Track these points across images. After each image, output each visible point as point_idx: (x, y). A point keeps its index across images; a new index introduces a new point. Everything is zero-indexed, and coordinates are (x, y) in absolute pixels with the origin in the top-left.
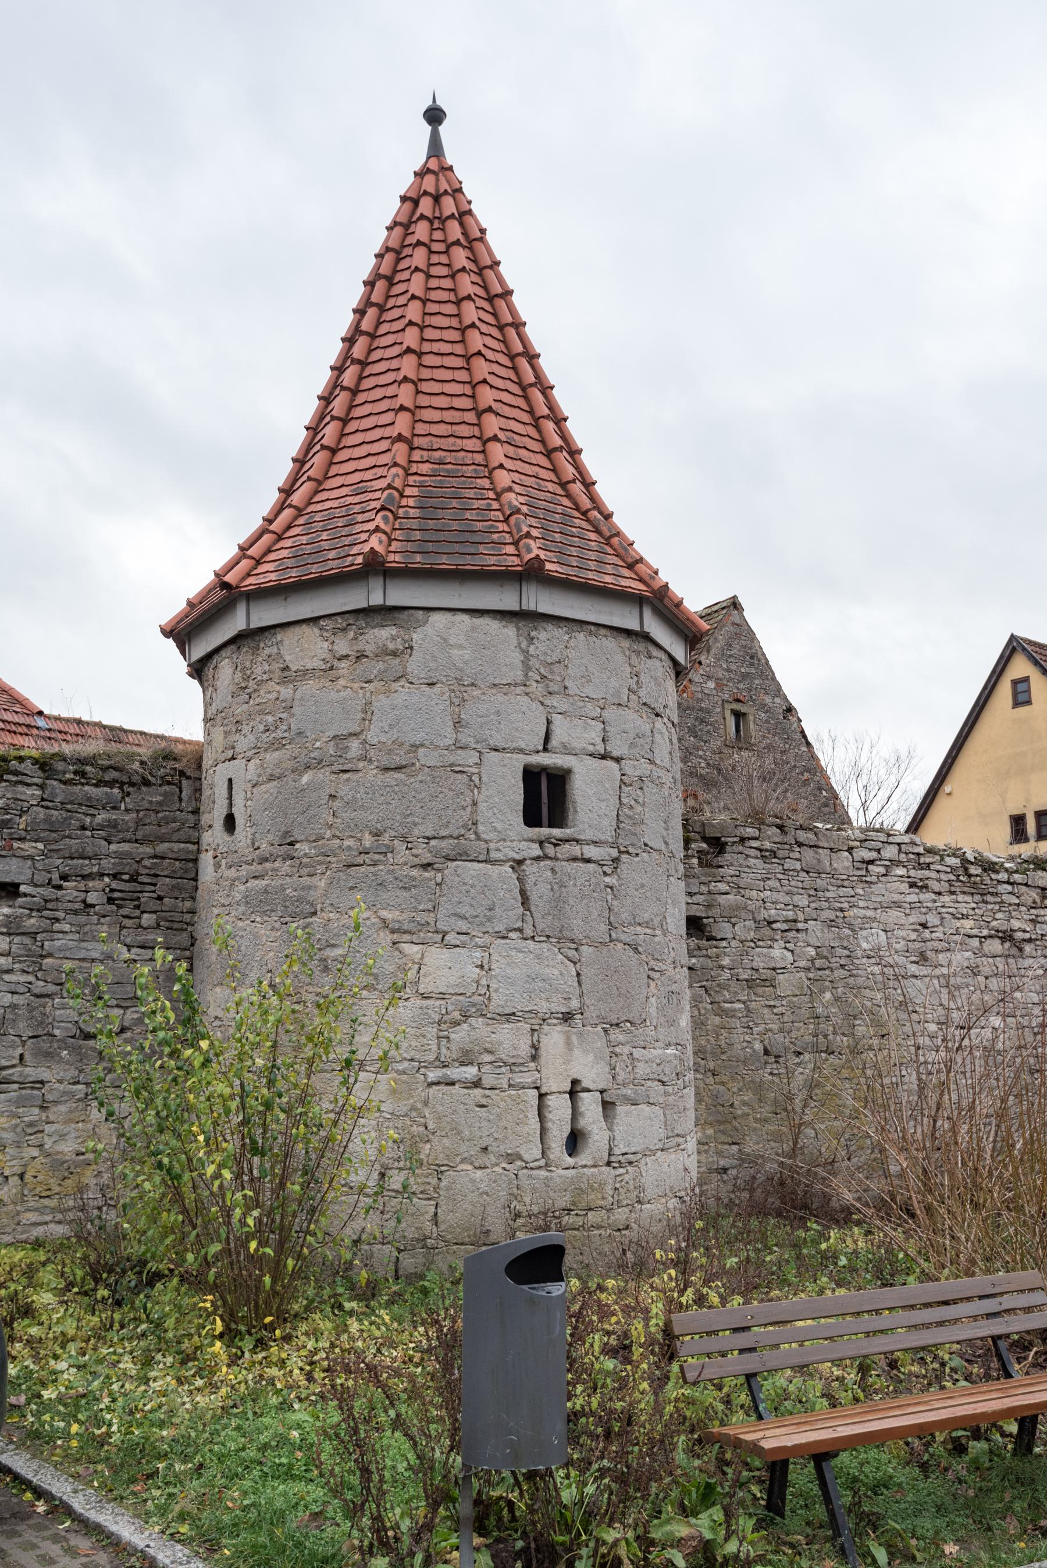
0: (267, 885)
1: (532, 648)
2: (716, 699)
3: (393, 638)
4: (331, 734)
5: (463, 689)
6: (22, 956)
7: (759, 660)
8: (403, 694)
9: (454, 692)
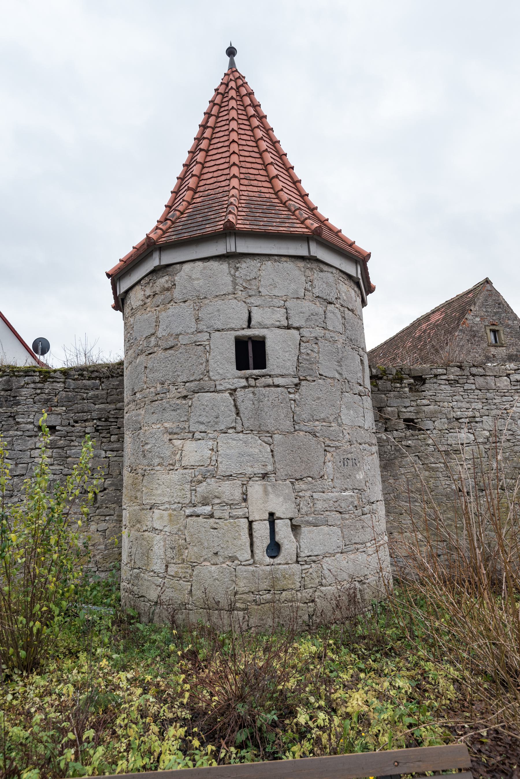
1: (237, 274)
2: (481, 325)
4: (144, 336)
5: (200, 301)
6: (58, 458)
7: (503, 305)
8: (173, 309)
9: (195, 303)
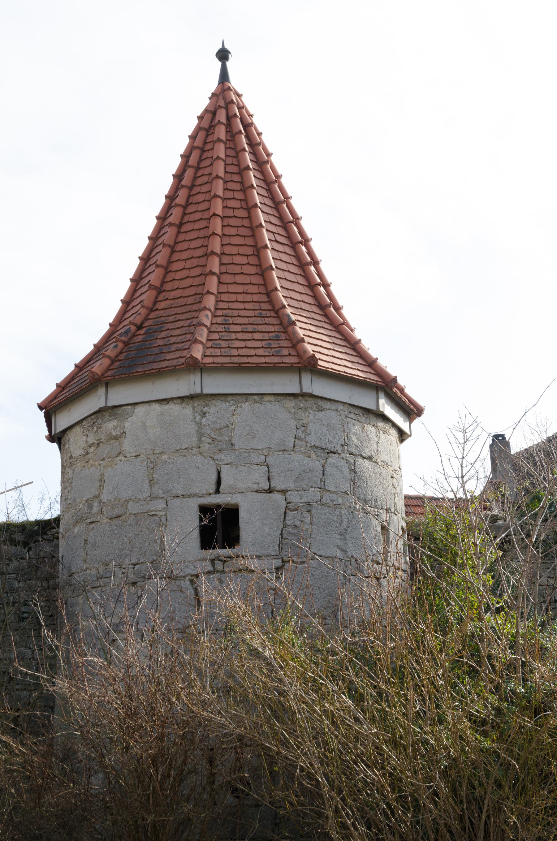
1: (204, 421)
3: (115, 428)
4: (85, 498)
5: (156, 456)
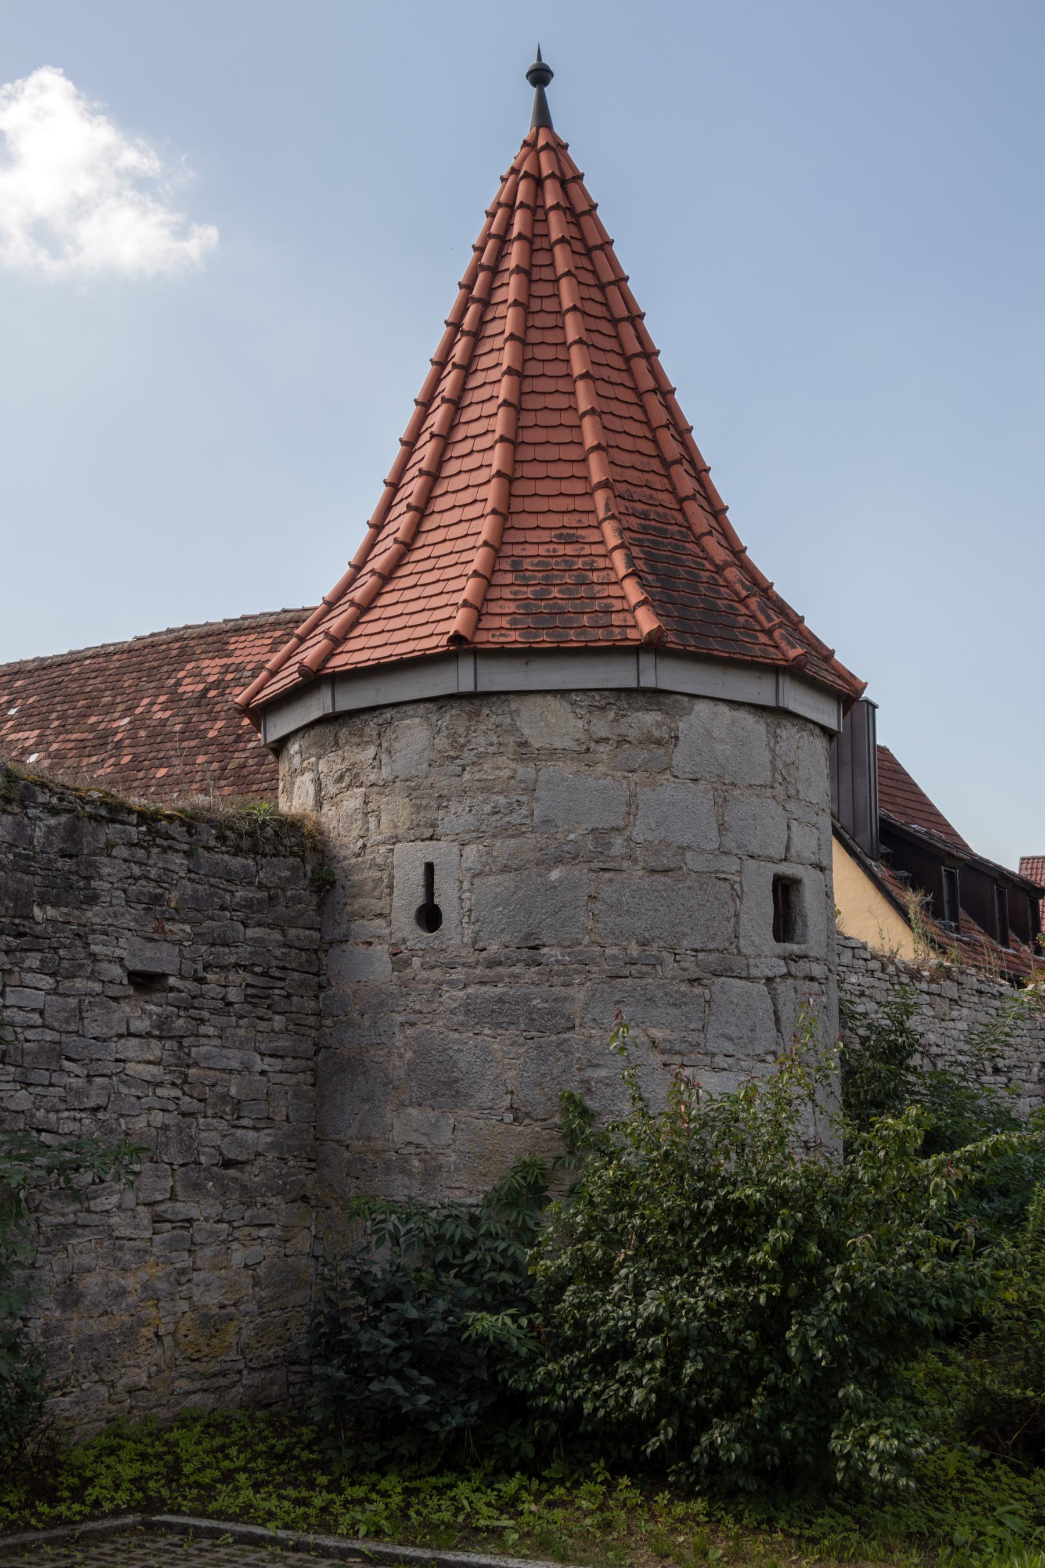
0: (504, 994)
3: (658, 725)
